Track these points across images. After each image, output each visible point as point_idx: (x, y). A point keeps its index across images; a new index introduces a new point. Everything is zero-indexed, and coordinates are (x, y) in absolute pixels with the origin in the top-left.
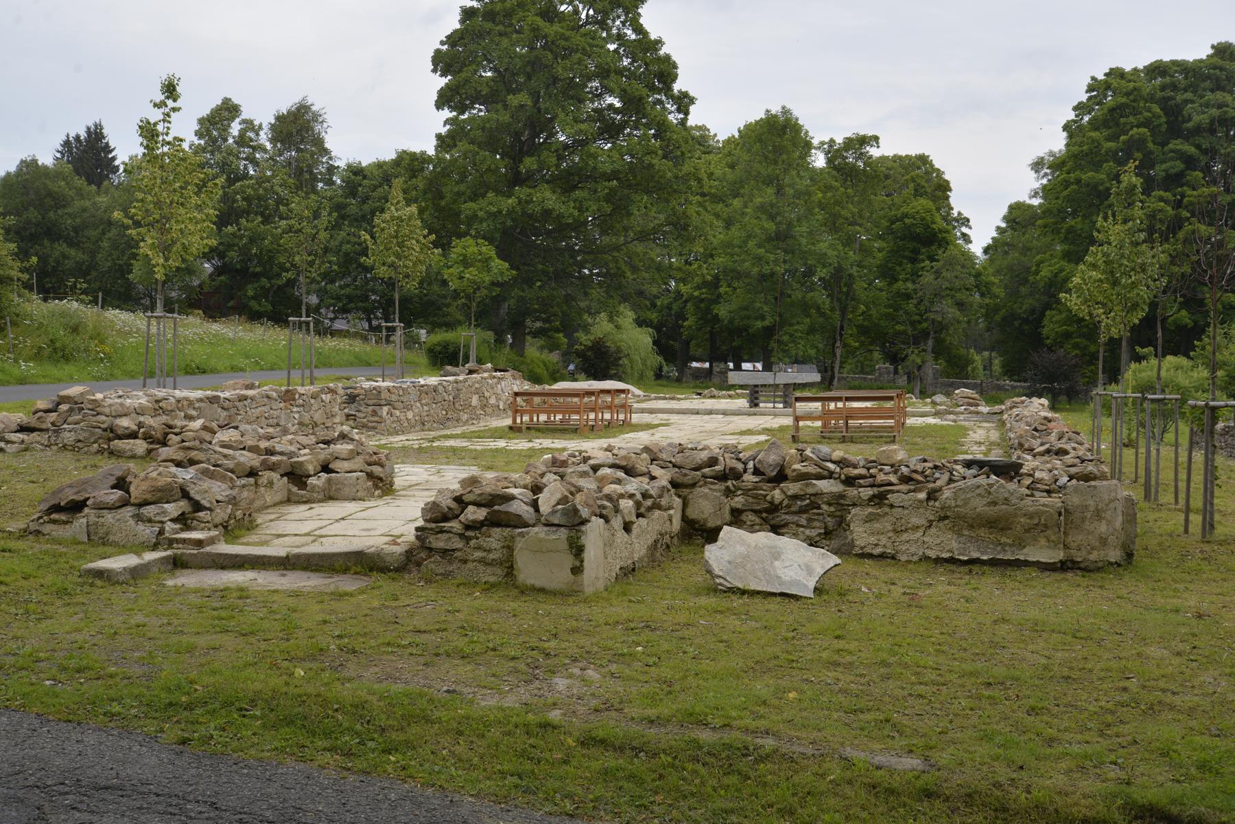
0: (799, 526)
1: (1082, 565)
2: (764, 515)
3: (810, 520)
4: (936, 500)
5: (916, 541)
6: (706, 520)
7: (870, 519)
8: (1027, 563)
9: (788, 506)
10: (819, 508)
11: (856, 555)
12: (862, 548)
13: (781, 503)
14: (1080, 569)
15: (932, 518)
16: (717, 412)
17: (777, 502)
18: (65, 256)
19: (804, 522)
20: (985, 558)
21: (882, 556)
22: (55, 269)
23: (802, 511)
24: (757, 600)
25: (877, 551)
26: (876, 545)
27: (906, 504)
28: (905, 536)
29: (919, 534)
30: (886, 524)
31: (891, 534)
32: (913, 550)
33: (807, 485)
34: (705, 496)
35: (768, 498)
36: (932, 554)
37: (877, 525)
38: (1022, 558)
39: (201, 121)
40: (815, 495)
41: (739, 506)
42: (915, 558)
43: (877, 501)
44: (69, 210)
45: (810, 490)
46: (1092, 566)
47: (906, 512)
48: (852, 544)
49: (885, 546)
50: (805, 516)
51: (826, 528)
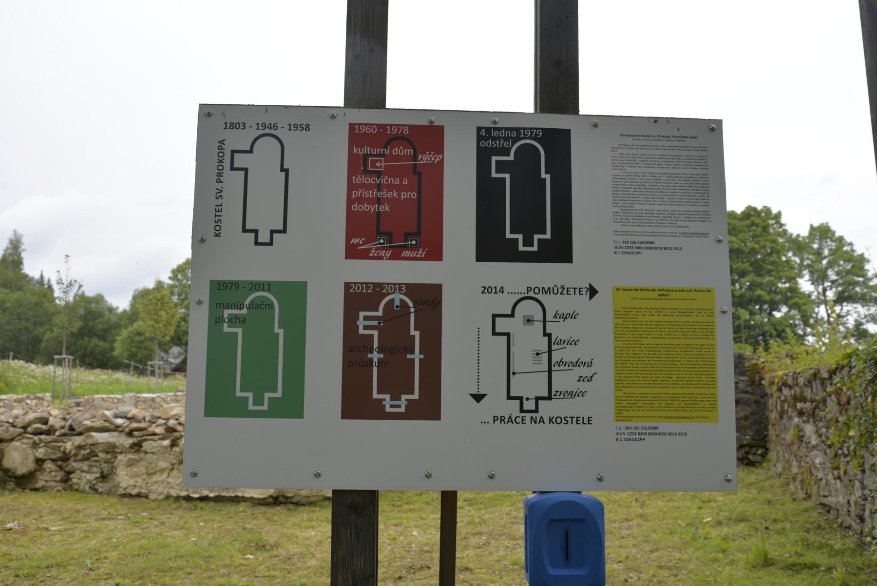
0: (82, 471)
1: (294, 500)
2: (59, 463)
3: (90, 466)
4: (177, 446)
5: (163, 482)
6: (16, 468)
7: (130, 464)
8: (244, 499)
9: (76, 455)
10: (97, 456)
11: (120, 495)
12: (125, 489)
13: (70, 452)
14: (292, 503)
15: (174, 461)
16: (635, 439)
17: (68, 451)
18: (97, 346)
19: (86, 468)
20: (212, 495)
21: (138, 495)
22: (91, 353)
23: (85, 459)
24: (463, 556)
25: (135, 492)
26: (135, 486)
27: (155, 450)
28: (155, 478)
29: (165, 476)
30: (141, 468)
31: (144, 476)
32: (160, 489)
33: (87, 437)
34: (16, 449)
35: (62, 449)
36: (174, 493)
37: (135, 469)
38: (240, 494)
39: (173, 271)
40: (93, 445)
41: (41, 456)
42: (162, 497)
43: (136, 448)
44: (101, 320)
45: (90, 441)
46: (304, 501)
47: (156, 457)
48: (117, 486)
49: (140, 487)
50: (87, 463)
51: (102, 473)
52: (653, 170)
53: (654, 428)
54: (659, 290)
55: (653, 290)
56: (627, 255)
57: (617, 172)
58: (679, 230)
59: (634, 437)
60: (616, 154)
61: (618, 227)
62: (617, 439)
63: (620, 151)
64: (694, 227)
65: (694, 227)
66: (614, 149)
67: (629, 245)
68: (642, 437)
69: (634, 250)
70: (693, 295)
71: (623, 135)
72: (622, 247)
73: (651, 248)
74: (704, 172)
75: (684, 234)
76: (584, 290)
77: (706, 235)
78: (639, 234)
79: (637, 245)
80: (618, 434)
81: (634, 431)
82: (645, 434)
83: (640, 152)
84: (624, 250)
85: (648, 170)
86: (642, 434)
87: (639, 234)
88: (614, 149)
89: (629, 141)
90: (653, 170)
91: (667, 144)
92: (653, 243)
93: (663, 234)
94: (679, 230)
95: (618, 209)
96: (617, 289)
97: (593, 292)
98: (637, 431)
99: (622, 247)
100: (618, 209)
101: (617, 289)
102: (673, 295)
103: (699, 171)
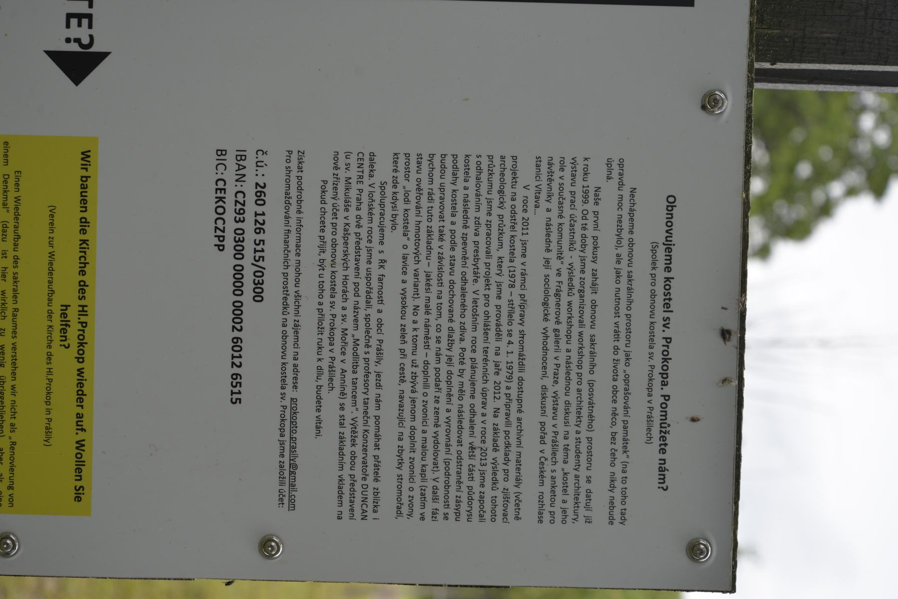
16: (220, 217)
52: (534, 311)
53: (258, 285)
54: (83, 311)
55: (83, 287)
56: (212, 196)
57: (526, 174)
58: (305, 396)
59: (230, 216)
60: (597, 177)
61: (318, 170)
62: (221, 152)
63: (610, 192)
64: (318, 457)
65: (318, 457)
66: (616, 168)
67: (251, 208)
68: (229, 243)
69: (231, 226)
70: (65, 433)
71: (671, 206)
72: (241, 178)
73: (238, 289)
74: (529, 508)
75: (289, 417)
76: (83, 34)
77: (288, 498)
78: (292, 247)
79: (250, 236)
80: (241, 157)
81: (249, 216)
82: (239, 253)
83: (606, 267)
84: (231, 188)
85: (535, 294)
86: (239, 242)
87: (292, 247)
88: (616, 168)
89: (649, 229)
90: (534, 311)
91: (639, 371)
92: (258, 297)
93: (290, 335)
94: (305, 396)
95: (384, 171)
96: (86, 155)
97: (78, 64)
98: (249, 226)
99: (241, 178)
100: (384, 171)
101: (86, 155)
102: (65, 360)
103: (530, 489)
